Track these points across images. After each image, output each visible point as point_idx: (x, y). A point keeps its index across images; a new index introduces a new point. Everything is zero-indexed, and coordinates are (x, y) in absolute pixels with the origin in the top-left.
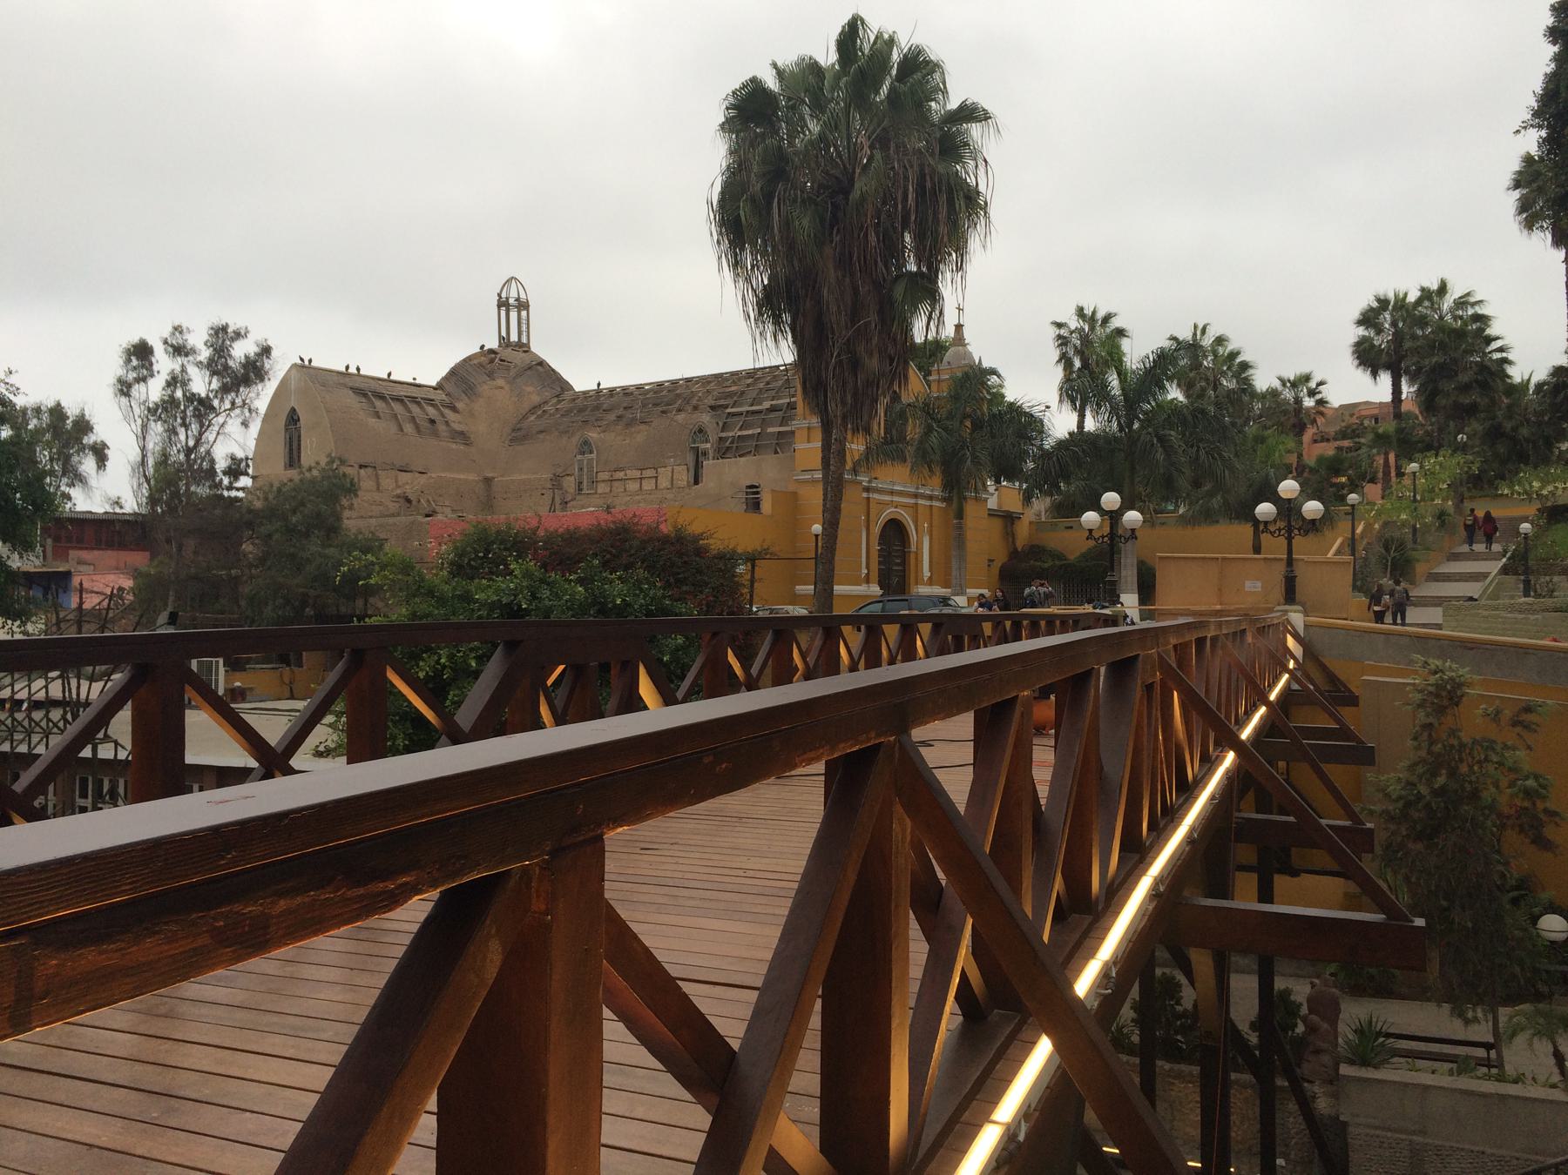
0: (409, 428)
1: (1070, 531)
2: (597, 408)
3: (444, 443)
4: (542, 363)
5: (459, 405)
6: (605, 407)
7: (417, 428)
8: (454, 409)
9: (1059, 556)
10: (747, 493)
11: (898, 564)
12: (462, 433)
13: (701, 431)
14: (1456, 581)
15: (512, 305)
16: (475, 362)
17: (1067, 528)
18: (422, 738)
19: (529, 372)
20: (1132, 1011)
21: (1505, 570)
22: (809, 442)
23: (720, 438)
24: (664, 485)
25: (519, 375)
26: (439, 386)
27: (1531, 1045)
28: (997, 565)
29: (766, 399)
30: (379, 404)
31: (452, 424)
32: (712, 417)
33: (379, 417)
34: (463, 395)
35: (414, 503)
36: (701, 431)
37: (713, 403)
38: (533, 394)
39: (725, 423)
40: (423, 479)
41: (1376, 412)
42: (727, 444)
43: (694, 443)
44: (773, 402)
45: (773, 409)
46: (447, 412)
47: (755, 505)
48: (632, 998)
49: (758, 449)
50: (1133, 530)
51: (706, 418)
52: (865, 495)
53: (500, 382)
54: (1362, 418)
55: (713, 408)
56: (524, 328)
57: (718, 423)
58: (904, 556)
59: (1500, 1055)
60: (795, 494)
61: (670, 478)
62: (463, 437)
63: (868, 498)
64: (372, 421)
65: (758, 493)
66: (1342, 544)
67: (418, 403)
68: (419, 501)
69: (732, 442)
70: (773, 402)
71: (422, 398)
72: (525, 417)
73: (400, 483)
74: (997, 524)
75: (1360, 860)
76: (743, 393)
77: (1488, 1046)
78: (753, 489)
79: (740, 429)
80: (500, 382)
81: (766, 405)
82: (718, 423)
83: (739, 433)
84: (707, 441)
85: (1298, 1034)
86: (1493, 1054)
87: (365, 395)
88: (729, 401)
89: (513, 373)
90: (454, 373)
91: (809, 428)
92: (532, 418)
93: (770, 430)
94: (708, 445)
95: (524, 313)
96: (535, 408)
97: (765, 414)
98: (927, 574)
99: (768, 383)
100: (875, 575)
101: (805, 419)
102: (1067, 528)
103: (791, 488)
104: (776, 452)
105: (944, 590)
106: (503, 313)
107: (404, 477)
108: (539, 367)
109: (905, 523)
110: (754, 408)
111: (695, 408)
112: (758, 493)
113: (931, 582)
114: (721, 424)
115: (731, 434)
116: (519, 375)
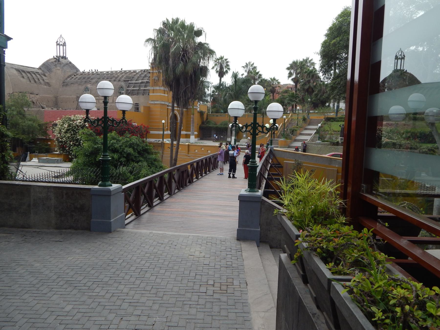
0: (32, 81)
1: (217, 117)
2: (89, 78)
3: (43, 86)
4: (70, 63)
5: (46, 74)
6: (92, 78)
7: (35, 82)
8: (45, 75)
10: (135, 105)
11: (175, 125)
12: (48, 83)
13: (121, 87)
14: (306, 135)
15: (61, 44)
16: (51, 61)
17: (217, 116)
18: (155, 173)
19: (67, 65)
21: (315, 133)
22: (153, 93)
23: (127, 90)
24: (111, 101)
25: (64, 66)
26: (40, 68)
29: (140, 80)
30: (23, 74)
31: (45, 80)
32: (124, 83)
33: (24, 78)
34: (48, 72)
35: (35, 103)
36: (121, 87)
37: (124, 79)
38: (69, 72)
39: (128, 85)
40: (38, 96)
41: (292, 87)
42: (129, 91)
43: (120, 90)
44: (142, 81)
45: (142, 83)
46: (43, 76)
49: (138, 94)
51: (123, 84)
52: (167, 107)
53: (58, 68)
54: (288, 88)
55: (125, 81)
56: (65, 52)
57: (126, 85)
61: (112, 100)
62: (48, 84)
63: (168, 108)
64: (22, 79)
65: (138, 106)
66: (282, 125)
67: (35, 74)
68: (37, 103)
69: (130, 91)
70: (142, 81)
71: (36, 72)
72: (66, 79)
73: (31, 97)
76: (133, 77)
79: (133, 88)
80: (58, 68)
81: (140, 81)
82: (126, 85)
83: (133, 89)
84: (123, 90)
87: (19, 71)
88: (130, 79)
89: (62, 65)
90: (44, 65)
91: (153, 90)
92: (69, 79)
93: (141, 88)
94: (124, 91)
95: (64, 47)
96: (69, 76)
97: (140, 84)
99: (140, 75)
100: (169, 129)
101: (152, 87)
102: (217, 116)
103: (148, 105)
104: (143, 95)
107: (32, 96)
108: (70, 64)
109: (177, 115)
110: (136, 82)
111: (119, 80)
112: (138, 106)
114: (127, 85)
115: (130, 89)
116: (64, 66)
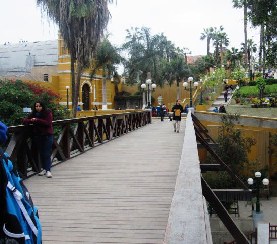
9: (129, 94)
20: (257, 27)
27: (246, 206)
28: (113, 96)
47: (47, 80)
48: (12, 182)
50: (154, 89)
58: (89, 94)
59: (238, 211)
60: (58, 77)
74: (113, 85)
75: (238, 176)
77: (236, 209)
78: (46, 75)
85: (124, 74)
86: (237, 211)
98: (95, 99)
103: (57, 75)
105: (82, 87)
106: (271, 233)
113: (96, 101)
